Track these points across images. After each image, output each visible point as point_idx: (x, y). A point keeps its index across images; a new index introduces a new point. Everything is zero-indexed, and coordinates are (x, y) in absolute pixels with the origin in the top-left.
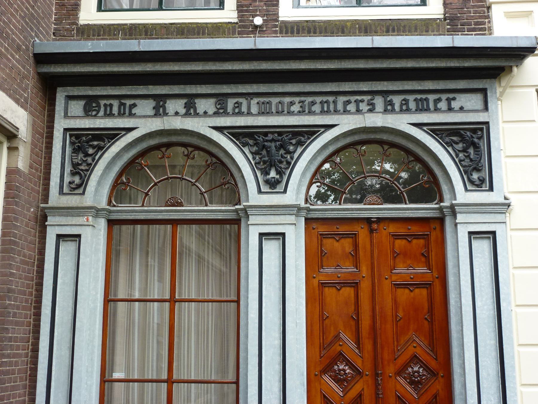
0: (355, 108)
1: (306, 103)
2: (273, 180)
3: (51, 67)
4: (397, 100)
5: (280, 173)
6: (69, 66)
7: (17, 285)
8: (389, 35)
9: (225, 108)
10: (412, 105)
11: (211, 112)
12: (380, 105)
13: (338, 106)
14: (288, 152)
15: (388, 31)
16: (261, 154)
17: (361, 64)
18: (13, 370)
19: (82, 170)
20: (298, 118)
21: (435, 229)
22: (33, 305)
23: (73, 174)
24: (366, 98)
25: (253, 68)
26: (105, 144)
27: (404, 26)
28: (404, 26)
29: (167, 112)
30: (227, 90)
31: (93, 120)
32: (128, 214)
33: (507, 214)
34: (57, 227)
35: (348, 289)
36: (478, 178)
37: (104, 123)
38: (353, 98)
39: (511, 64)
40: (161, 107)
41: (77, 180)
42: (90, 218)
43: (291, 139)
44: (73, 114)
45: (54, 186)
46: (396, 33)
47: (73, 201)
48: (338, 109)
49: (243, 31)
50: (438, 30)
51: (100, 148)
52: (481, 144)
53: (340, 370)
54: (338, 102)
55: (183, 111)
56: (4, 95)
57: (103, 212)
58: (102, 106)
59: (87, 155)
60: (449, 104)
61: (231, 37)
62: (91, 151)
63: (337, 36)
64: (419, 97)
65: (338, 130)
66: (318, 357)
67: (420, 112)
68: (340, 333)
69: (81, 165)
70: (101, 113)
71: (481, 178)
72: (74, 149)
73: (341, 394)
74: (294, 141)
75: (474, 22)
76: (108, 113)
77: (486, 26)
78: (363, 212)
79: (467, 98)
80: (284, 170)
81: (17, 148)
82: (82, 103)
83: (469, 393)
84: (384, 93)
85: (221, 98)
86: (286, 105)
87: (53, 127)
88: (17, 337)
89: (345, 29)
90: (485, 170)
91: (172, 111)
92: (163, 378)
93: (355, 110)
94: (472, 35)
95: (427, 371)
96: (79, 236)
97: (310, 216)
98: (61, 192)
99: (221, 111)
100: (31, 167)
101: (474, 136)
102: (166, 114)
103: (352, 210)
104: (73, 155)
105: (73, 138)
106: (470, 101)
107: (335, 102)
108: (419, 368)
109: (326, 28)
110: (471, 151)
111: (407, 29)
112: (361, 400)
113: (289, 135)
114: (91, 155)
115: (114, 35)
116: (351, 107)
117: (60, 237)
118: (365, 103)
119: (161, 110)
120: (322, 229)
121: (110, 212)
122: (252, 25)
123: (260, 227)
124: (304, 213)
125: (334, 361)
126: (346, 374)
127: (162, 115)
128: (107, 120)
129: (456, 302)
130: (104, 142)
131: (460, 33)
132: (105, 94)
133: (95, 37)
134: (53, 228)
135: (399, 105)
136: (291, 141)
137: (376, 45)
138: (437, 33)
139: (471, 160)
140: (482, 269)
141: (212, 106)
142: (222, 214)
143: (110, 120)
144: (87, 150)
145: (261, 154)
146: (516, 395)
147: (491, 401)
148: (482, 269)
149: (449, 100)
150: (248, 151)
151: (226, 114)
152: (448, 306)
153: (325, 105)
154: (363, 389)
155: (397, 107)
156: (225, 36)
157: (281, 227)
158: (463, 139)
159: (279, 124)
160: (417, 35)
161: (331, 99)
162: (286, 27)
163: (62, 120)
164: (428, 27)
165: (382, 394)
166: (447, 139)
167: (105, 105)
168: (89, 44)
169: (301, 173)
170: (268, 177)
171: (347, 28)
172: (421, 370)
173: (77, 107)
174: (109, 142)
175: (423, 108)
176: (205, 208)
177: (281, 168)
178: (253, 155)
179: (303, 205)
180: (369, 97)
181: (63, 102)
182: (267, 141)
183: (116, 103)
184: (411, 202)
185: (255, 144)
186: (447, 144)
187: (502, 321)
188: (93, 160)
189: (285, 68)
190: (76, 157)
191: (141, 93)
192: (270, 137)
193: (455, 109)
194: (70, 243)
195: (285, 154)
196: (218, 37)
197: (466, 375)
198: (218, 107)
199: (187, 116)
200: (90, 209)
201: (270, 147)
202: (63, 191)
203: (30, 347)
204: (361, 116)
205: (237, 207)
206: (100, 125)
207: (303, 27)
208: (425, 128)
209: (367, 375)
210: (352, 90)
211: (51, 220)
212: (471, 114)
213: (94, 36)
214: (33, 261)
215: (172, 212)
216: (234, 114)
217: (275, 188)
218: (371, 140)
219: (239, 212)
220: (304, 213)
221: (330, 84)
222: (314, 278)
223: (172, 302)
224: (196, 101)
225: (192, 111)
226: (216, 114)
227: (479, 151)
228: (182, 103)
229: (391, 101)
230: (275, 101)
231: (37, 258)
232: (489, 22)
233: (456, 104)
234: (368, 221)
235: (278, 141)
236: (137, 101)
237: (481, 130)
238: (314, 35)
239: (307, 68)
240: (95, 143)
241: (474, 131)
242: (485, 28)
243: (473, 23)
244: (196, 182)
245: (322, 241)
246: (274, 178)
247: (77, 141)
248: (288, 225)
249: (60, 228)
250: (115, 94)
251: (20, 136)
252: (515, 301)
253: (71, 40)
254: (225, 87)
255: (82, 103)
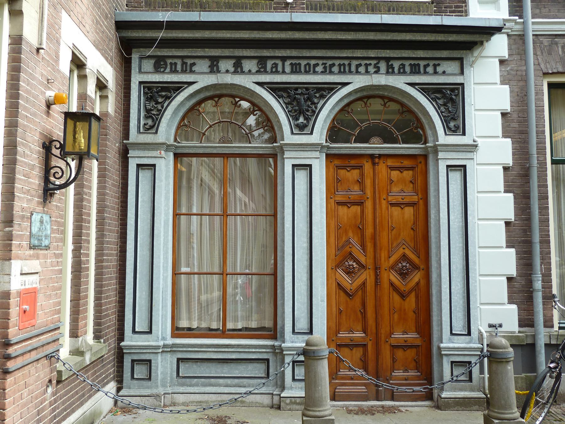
0: (365, 70)
1: (328, 65)
2: (302, 124)
3: (128, 32)
4: (396, 65)
5: (307, 119)
6: (143, 31)
7: (110, 202)
8: (390, 14)
9: (265, 67)
10: (408, 69)
11: (254, 70)
12: (383, 68)
13: (352, 68)
14: (313, 103)
15: (389, 11)
16: (293, 104)
17: (298, 35)
18: (109, 265)
19: (154, 115)
20: (321, 77)
21: (421, 163)
22: (120, 217)
23: (146, 117)
24: (373, 62)
25: (288, 37)
26: (172, 94)
27: (402, 8)
28: (402, 8)
29: (220, 70)
30: (266, 53)
31: (162, 75)
32: (190, 149)
33: (475, 153)
34: (136, 159)
35: (356, 207)
36: (454, 125)
37: (171, 78)
38: (364, 62)
39: (483, 40)
40: (215, 65)
41: (150, 122)
42: (163, 152)
43: (315, 93)
44: (145, 70)
45: (133, 126)
46: (395, 12)
47: (148, 138)
48: (352, 70)
49: (277, 6)
50: (427, 12)
51: (167, 98)
52: (457, 100)
53: (349, 265)
54: (352, 65)
55: (232, 69)
56: (99, 53)
57: (172, 147)
58: (168, 64)
59: (157, 103)
60: (367, 69)
61: (268, 12)
62: (160, 100)
63: (350, 13)
64: (413, 62)
65: (352, 86)
66: (334, 256)
67: (414, 75)
68: (350, 238)
69: (152, 110)
70: (168, 70)
71: (457, 126)
72: (147, 98)
73: (350, 282)
74: (317, 95)
75: (454, 5)
76: (173, 70)
77: (464, 9)
78: (369, 150)
79: (448, 65)
80: (310, 117)
81: (107, 97)
82: (152, 61)
83: (443, 281)
84: (387, 59)
85: (262, 61)
86: (312, 66)
87: (130, 81)
88: (111, 241)
89: (357, 8)
90: (460, 120)
91: (223, 69)
92: (215, 271)
93: (364, 72)
94: (452, 15)
95: (412, 266)
96: (154, 166)
97: (329, 152)
98: (139, 132)
99: (262, 70)
100: (116, 112)
101: (452, 93)
102: (219, 71)
103: (361, 148)
104: (147, 102)
105: (146, 90)
106: (450, 67)
107: (350, 65)
108: (406, 263)
109: (342, 6)
110: (449, 105)
111: (404, 9)
112: (364, 287)
113: (314, 90)
114: (161, 103)
115: (176, 7)
116: (362, 69)
117: (139, 166)
118: (372, 66)
119: (215, 68)
120: (337, 162)
121: (177, 147)
122: (284, 2)
123: (293, 160)
124: (325, 150)
125: (345, 259)
126: (354, 268)
127: (216, 71)
128: (173, 75)
129: (435, 216)
130: (171, 93)
131: (444, 14)
132: (170, 55)
133: (160, 9)
134: (133, 159)
135: (397, 69)
136: (316, 95)
137: (384, 21)
138: (426, 13)
139: (450, 112)
140: (455, 192)
141: (255, 66)
142: (263, 150)
143: (176, 75)
144: (158, 98)
145: (293, 104)
146: (476, 282)
147: (458, 286)
148: (455, 192)
149: (435, 66)
150: (282, 101)
151: (266, 72)
152: (429, 219)
153: (342, 67)
154: (366, 279)
155: (396, 70)
156: (263, 10)
157: (308, 160)
158: (444, 96)
159: (307, 82)
160: (412, 14)
161: (346, 62)
162: (311, 5)
163: (138, 75)
164: (419, 8)
165: (380, 282)
166: (433, 96)
167: (171, 63)
168: (160, 14)
169: (324, 119)
170: (298, 122)
171: (358, 7)
172: (408, 265)
173: (148, 65)
174: (174, 93)
175: (415, 70)
176: (250, 145)
177: (308, 115)
178: (286, 105)
179: (325, 144)
180: (375, 62)
181: (138, 60)
182: (297, 94)
183: (179, 62)
184: (404, 142)
185: (288, 96)
186: (432, 100)
187: (468, 230)
188: (162, 107)
189: (313, 37)
190: (149, 104)
191: (199, 55)
192: (300, 91)
193: (439, 73)
194: (147, 171)
195: (311, 104)
196: (258, 12)
197: (442, 268)
198: (260, 67)
199: (235, 74)
200: (162, 145)
201: (300, 99)
202: (140, 130)
203: (119, 249)
204: (369, 76)
205: (275, 144)
206: (168, 79)
207: (324, 5)
208: (417, 87)
209: (369, 269)
210: (363, 56)
211: (131, 153)
212: (451, 77)
213: (159, 7)
214: (118, 184)
215: (224, 148)
216: (272, 72)
217: (303, 130)
218: (375, 95)
219: (276, 148)
220: (325, 150)
221: (346, 50)
222: (331, 198)
223: (225, 216)
224: (242, 62)
225: (239, 70)
226: (258, 72)
227: (456, 105)
228: (231, 63)
229: (392, 65)
230: (303, 63)
231: (121, 182)
232: (466, 6)
233: (440, 69)
234: (372, 156)
235: (306, 94)
236: (196, 61)
237: (458, 89)
238: (333, 11)
239: (330, 38)
240: (164, 94)
241: (452, 90)
242: (463, 10)
243: (453, 6)
244: (242, 125)
245: (337, 171)
246: (303, 123)
247: (149, 92)
248: (314, 159)
249: (139, 159)
250: (179, 55)
251: (109, 87)
252: (478, 216)
253: (141, 11)
254: (277, 51)
255: (152, 61)
